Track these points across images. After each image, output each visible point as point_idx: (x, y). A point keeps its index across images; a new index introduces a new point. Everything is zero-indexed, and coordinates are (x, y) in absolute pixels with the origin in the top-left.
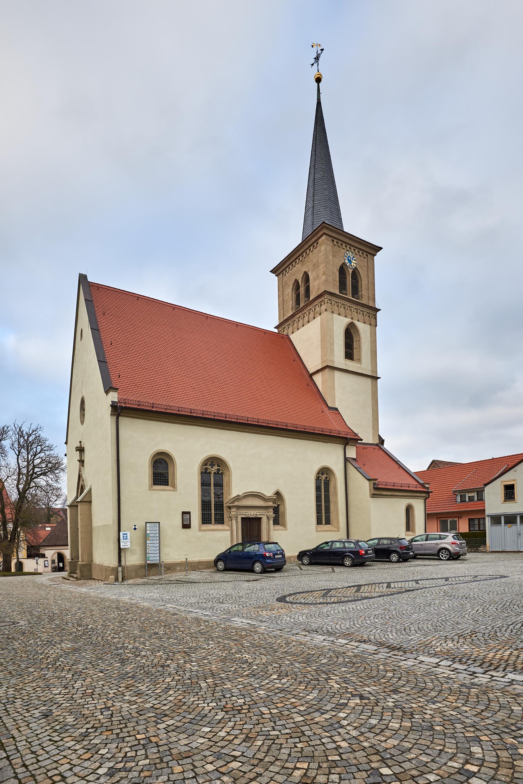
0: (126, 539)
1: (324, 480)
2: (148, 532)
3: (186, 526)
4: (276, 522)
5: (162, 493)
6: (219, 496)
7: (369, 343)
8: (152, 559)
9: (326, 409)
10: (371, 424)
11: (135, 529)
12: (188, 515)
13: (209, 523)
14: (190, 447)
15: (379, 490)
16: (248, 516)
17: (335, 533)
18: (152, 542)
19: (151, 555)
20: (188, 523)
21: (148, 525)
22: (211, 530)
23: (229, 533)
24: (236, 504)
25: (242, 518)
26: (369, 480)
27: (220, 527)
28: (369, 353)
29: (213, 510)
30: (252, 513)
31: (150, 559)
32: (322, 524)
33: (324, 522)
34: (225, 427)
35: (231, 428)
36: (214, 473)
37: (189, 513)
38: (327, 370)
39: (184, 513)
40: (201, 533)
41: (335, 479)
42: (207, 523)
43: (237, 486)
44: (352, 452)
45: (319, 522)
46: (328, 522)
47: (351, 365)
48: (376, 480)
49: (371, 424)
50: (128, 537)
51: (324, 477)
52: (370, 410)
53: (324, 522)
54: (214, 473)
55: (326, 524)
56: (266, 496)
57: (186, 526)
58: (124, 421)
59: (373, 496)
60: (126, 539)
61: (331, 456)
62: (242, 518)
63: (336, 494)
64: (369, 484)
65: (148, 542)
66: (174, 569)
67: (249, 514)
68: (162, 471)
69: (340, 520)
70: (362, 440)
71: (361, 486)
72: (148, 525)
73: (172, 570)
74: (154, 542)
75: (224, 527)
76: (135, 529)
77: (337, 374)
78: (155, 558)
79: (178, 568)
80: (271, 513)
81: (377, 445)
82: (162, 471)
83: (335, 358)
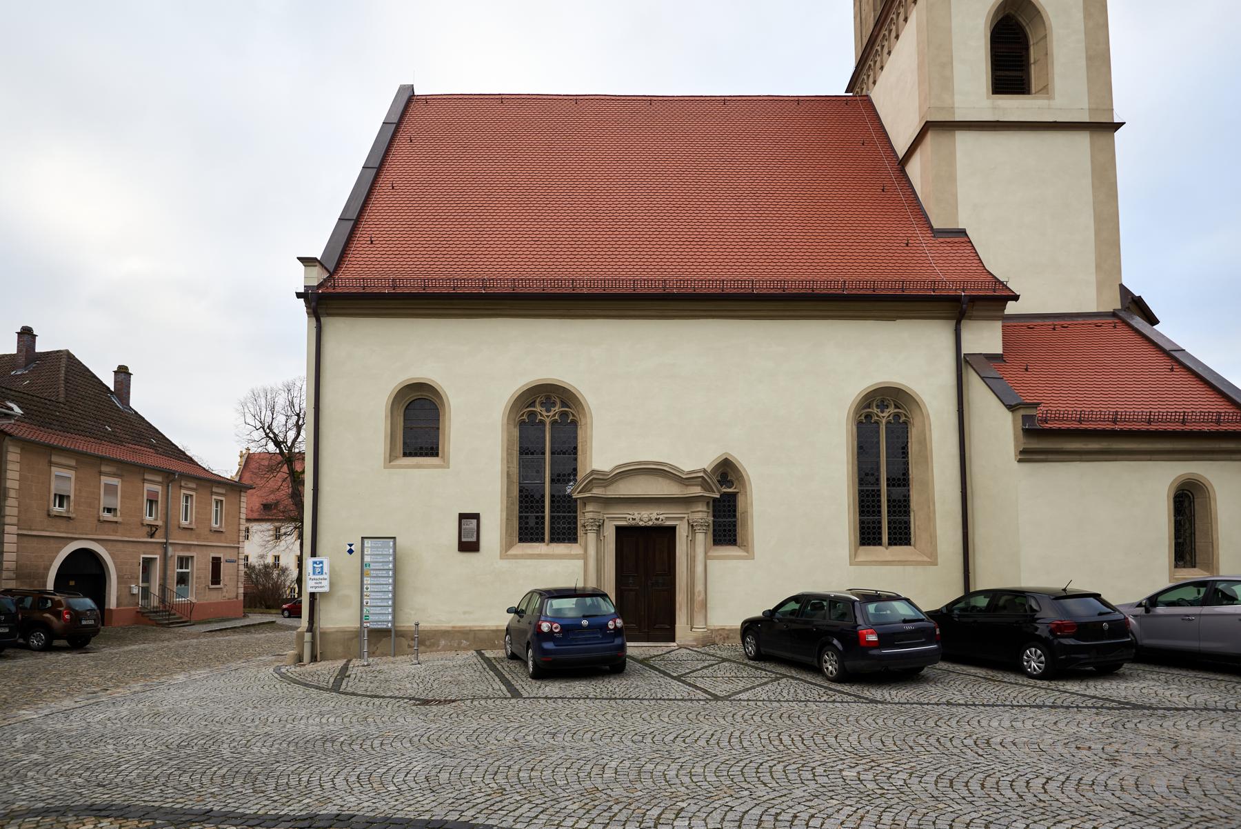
0: (321, 573)
1: (883, 426)
2: (367, 559)
3: (469, 546)
4: (468, 518)
5: (420, 471)
6: (566, 474)
7: (1083, 36)
8: (376, 618)
9: (922, 237)
10: (1091, 257)
11: (351, 552)
12: (475, 521)
13: (537, 540)
14: (480, 370)
15: (1045, 439)
16: (633, 523)
17: (920, 569)
18: (376, 581)
19: (373, 610)
20: (474, 539)
21: (368, 543)
22: (532, 557)
23: (580, 563)
24: (597, 492)
25: (618, 528)
26: (1011, 408)
27: (899, 551)
28: (1083, 63)
29: (546, 506)
30: (645, 516)
31: (371, 618)
32: (880, 544)
33: (547, 537)
34: (572, 312)
35: (590, 312)
36: (546, 423)
37: (476, 516)
38: (930, 138)
39: (463, 517)
40: (505, 564)
41: (925, 417)
42: (532, 540)
43: (602, 451)
44: (985, 338)
45: (868, 535)
46: (901, 536)
47: (1013, 107)
48: (1035, 405)
49: (1092, 257)
50: (326, 569)
51: (884, 416)
52: (1086, 221)
53: (547, 537)
54: (546, 423)
55: (890, 544)
56: (682, 472)
57: (469, 546)
58: (340, 330)
59: (1026, 455)
60: (321, 573)
61: (914, 358)
62: (618, 528)
63: (926, 459)
64: (1014, 420)
65: (367, 580)
66: (432, 645)
67: (637, 516)
68: (419, 422)
69: (939, 532)
70: (1153, 320)
71: (996, 426)
72: (368, 543)
73: (429, 647)
74: (382, 581)
75: (575, 549)
76: (351, 552)
77: (963, 139)
78: (382, 618)
79: (443, 642)
80: (702, 514)
81: (1114, 314)
82: (419, 422)
83: (957, 98)
